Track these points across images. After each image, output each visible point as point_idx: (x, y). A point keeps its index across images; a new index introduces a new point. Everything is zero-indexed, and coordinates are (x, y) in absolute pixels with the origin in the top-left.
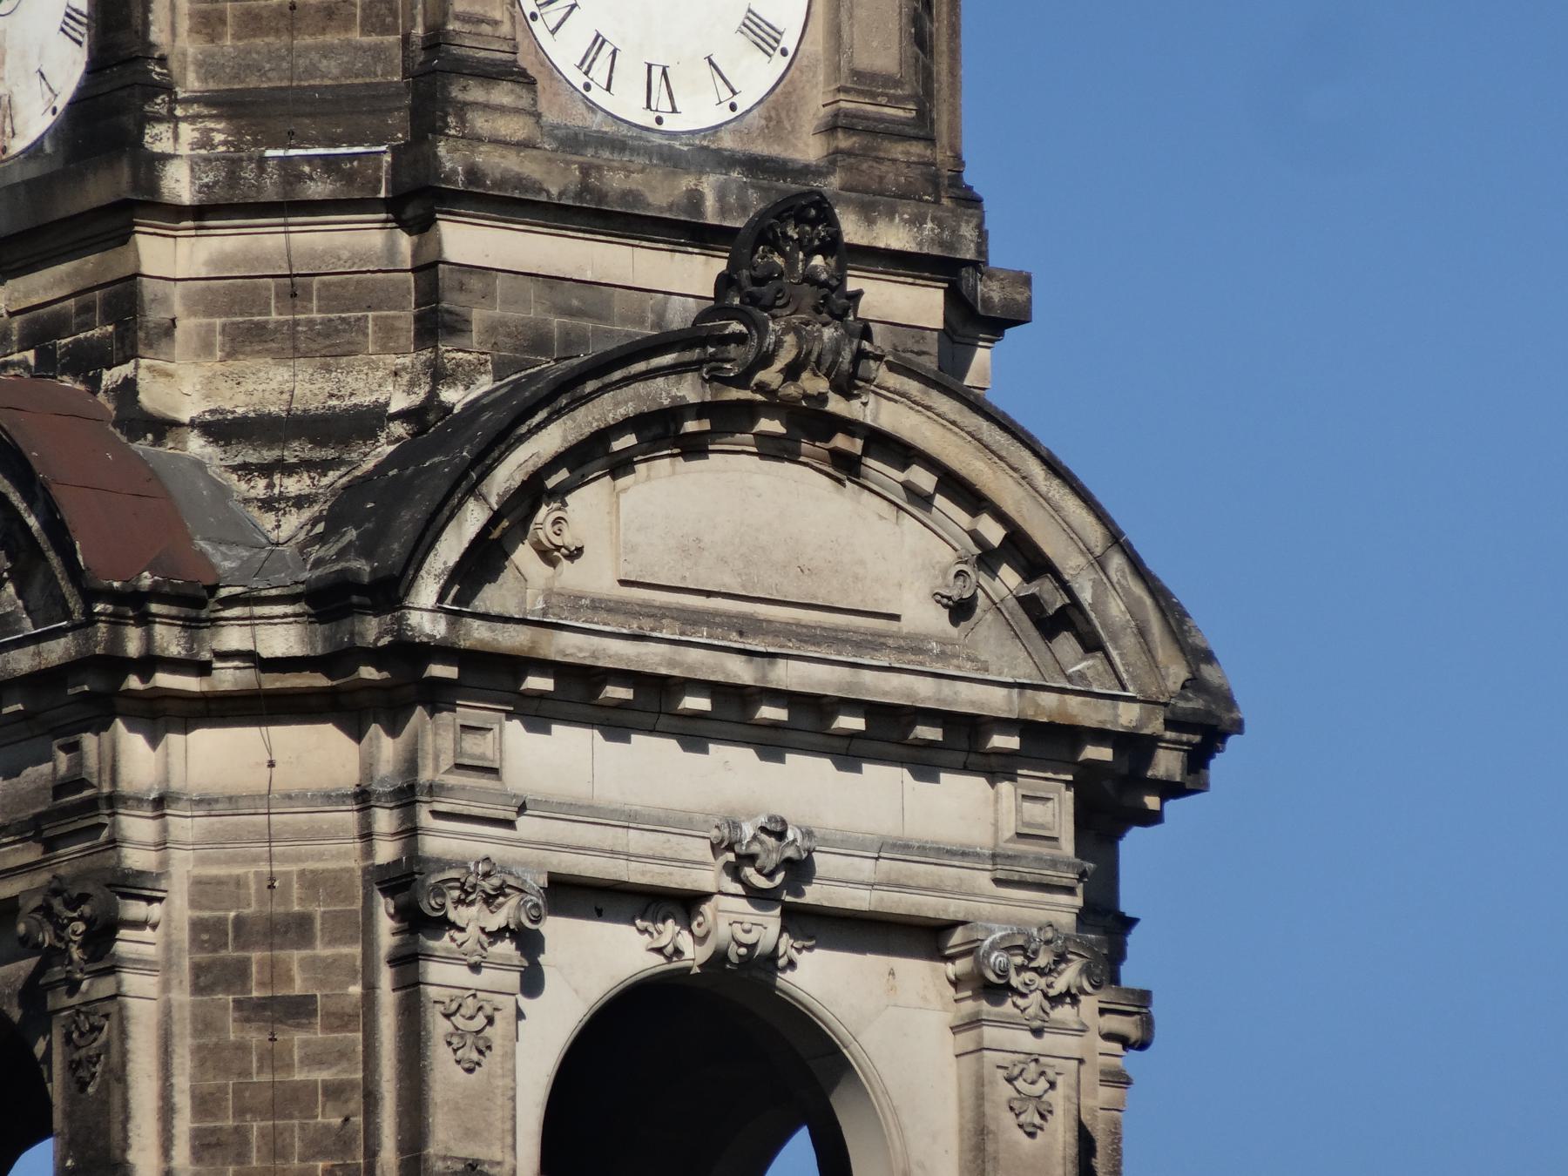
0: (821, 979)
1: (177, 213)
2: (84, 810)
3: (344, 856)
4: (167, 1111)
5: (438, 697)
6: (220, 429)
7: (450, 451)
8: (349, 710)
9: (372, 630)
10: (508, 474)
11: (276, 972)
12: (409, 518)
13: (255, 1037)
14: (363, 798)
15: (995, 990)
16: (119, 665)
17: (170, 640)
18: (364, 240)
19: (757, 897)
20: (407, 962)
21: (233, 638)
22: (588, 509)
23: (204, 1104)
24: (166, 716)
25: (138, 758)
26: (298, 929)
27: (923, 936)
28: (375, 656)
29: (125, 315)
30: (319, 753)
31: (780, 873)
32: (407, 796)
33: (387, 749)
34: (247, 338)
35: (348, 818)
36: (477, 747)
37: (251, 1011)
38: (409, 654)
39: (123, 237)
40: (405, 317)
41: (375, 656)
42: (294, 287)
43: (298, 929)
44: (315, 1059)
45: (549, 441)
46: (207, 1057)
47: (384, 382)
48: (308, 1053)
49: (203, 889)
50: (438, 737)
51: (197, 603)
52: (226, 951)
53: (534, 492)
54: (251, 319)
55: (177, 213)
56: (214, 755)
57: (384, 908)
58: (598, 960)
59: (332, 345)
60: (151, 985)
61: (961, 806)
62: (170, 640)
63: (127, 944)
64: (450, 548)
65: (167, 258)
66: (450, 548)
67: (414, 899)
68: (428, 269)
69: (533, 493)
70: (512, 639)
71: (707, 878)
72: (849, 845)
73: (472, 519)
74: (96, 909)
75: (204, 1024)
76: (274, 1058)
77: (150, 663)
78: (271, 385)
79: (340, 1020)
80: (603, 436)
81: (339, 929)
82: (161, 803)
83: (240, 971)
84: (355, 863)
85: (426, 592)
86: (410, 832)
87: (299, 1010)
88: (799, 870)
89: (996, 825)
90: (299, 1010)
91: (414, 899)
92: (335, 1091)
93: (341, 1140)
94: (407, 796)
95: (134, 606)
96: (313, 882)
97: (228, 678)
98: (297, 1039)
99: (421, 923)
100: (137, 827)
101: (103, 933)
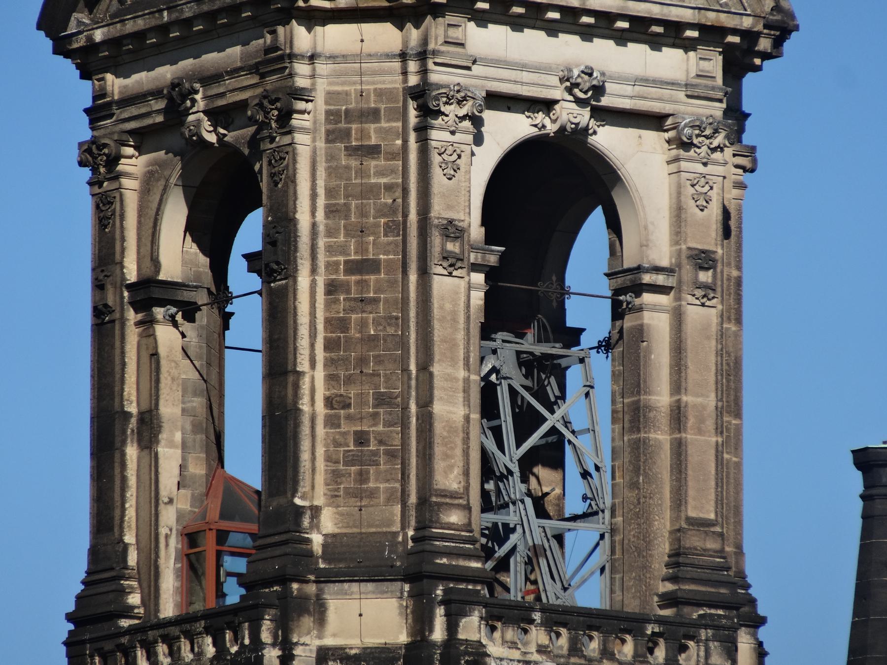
0: (608, 139)
2: (278, 60)
3: (394, 82)
4: (314, 196)
11: (363, 134)
13: (354, 163)
14: (403, 56)
15: (686, 145)
19: (579, 102)
20: (422, 130)
23: (330, 193)
25: (302, 38)
26: (374, 115)
27: (654, 121)
30: (384, 36)
31: (591, 92)
32: (423, 56)
33: (414, 35)
35: (397, 65)
36: (454, 34)
37: (353, 151)
43: (374, 115)
44: (380, 173)
46: (332, 172)
49: (331, 97)
50: (437, 29)
52: (340, 125)
56: (336, 37)
57: (412, 105)
58: (508, 130)
60: (307, 140)
61: (671, 62)
63: (297, 121)
67: (425, 101)
71: (557, 93)
72: (621, 79)
74: (283, 105)
75: (331, 157)
76: (362, 172)
79: (392, 156)
81: (392, 115)
82: (312, 58)
83: (347, 133)
84: (399, 86)
86: (424, 72)
87: (373, 151)
88: (599, 90)
89: (687, 71)
90: (373, 151)
91: (425, 101)
92: (389, 188)
94: (423, 56)
98: (372, 164)
99: (428, 113)
100: (302, 68)
101: (286, 116)
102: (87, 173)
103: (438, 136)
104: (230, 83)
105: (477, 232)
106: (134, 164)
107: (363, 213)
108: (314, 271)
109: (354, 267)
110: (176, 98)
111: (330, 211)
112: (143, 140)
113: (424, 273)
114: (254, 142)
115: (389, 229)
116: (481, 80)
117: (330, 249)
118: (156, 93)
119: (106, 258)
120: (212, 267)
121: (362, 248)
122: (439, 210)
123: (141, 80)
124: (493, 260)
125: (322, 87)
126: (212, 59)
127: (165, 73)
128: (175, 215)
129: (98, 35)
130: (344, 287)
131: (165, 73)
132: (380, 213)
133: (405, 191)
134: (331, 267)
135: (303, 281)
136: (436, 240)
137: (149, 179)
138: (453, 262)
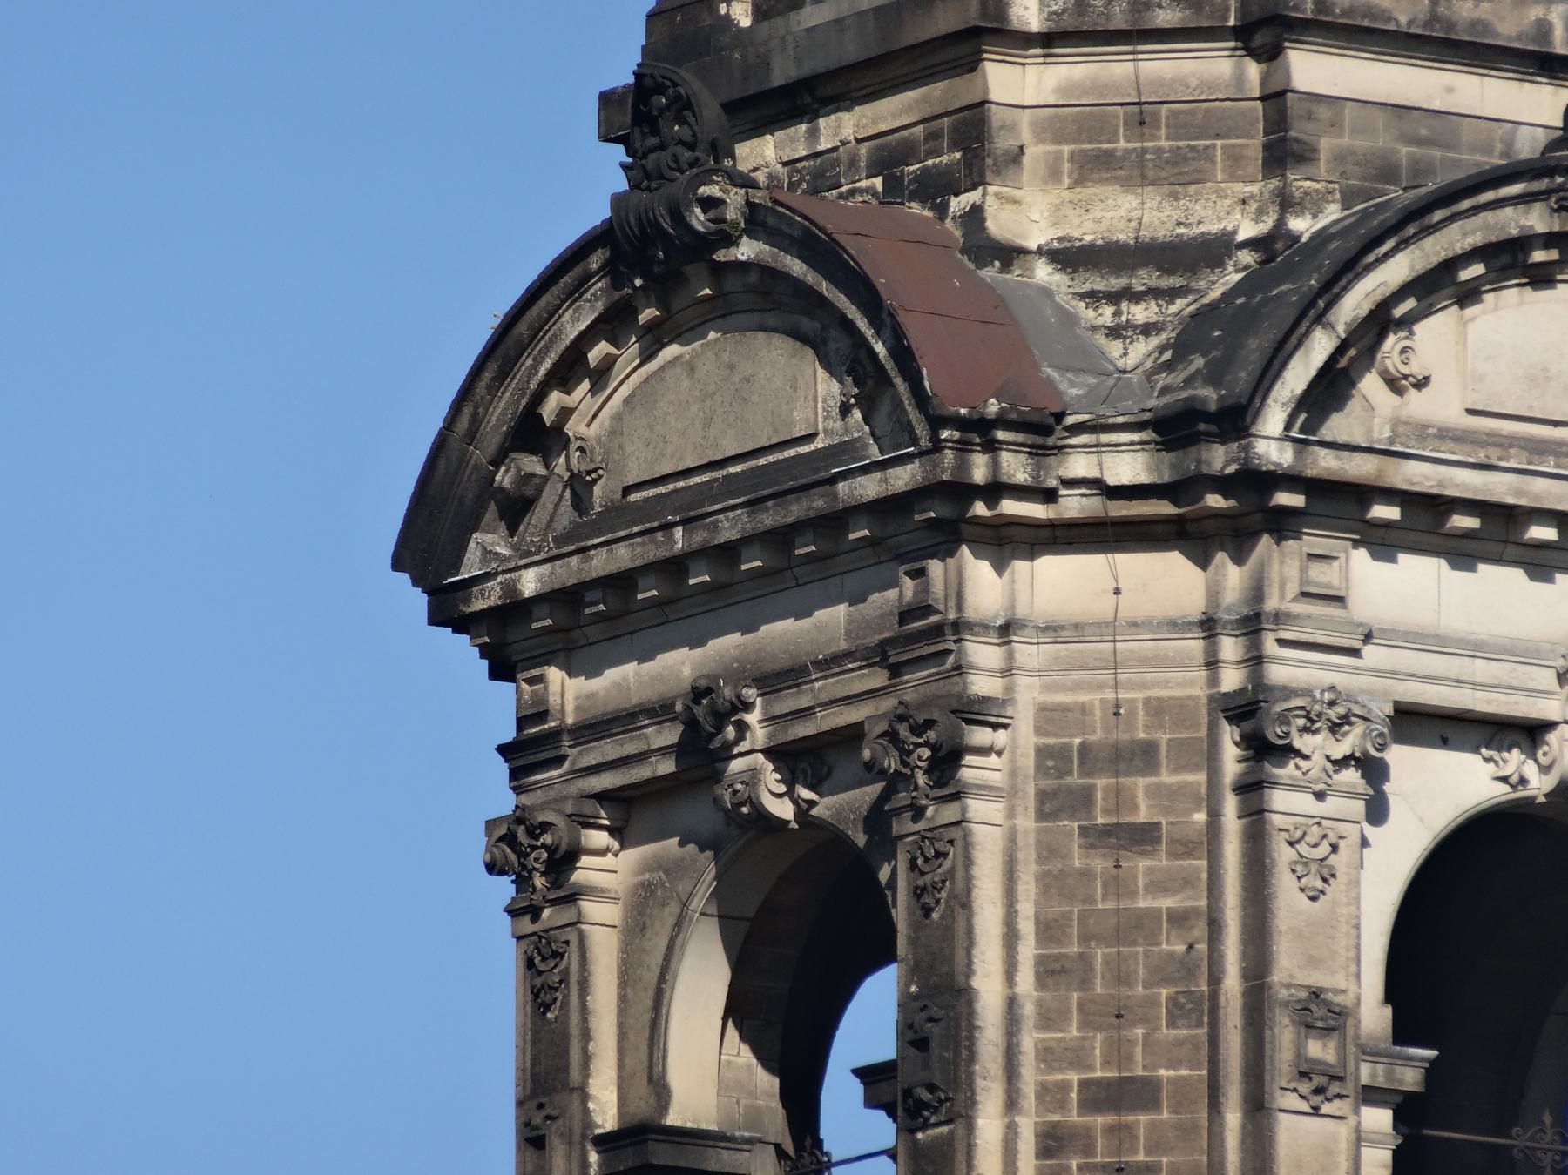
1: (1026, 40)
2: (924, 639)
3: (1189, 684)
4: (1011, 938)
5: (1283, 525)
6: (1068, 257)
7: (1296, 279)
8: (1193, 537)
9: (1219, 458)
10: (1356, 302)
11: (1121, 801)
12: (1256, 346)
13: (1100, 864)
14: (1209, 626)
16: (964, 492)
17: (1016, 468)
18: (1213, 69)
20: (1252, 789)
21: (1079, 466)
22: (1434, 339)
23: (1048, 930)
24: (1011, 542)
25: (983, 584)
26: (1143, 756)
28: (1222, 484)
29: (973, 139)
30: (1165, 580)
32: (1252, 624)
33: (1233, 577)
34: (1095, 166)
35: (1194, 645)
36: (1324, 576)
37: (1097, 838)
38: (1255, 482)
39: (972, 64)
40: (1254, 145)
41: (1222, 484)
42: (1141, 115)
43: (1143, 756)
44: (1159, 886)
45: (1396, 270)
46: (1051, 883)
47: (1231, 210)
48: (1153, 887)
49: (1048, 716)
50: (1284, 565)
51: (1043, 430)
52: (1072, 778)
53: (1380, 322)
54: (1099, 146)
55: (1026, 40)
56: (1060, 582)
57: (1229, 736)
59: (1179, 172)
62: (1016, 468)
63: (972, 770)
64: (1297, 376)
65: (1014, 85)
66: (1297, 376)
67: (1258, 726)
68: (1276, 98)
69: (1380, 322)
70: (1359, 468)
73: (1319, 348)
74: (937, 744)
75: (1048, 851)
76: (1119, 885)
77: (995, 490)
78: (1119, 213)
79: (1184, 848)
80: (1450, 265)
81: (1184, 757)
82: (1007, 630)
85: (1273, 420)
86: (1255, 660)
87: (1143, 837)
90: (1143, 837)
91: (1258, 726)
92: (1179, 919)
93: (1185, 968)
94: (1252, 624)
95: (980, 431)
96: (1157, 709)
97: (1074, 505)
98: (1142, 866)
99: (1264, 750)
100: (983, 653)
101: (947, 760)
102: (505, 888)
103: (1287, 803)
104: (825, 687)
105: (1374, 1016)
106: (609, 867)
107: (1121, 977)
108: (1012, 1104)
109: (1100, 1096)
110: (704, 722)
111: (1048, 972)
112: (630, 811)
113: (1258, 1107)
114: (877, 819)
115: (1178, 1011)
116: (1382, 679)
117: (1047, 1056)
118: (659, 711)
119: (547, 1079)
120: (786, 1096)
121: (1118, 1052)
122: (1290, 968)
123: (624, 679)
124: (1411, 1078)
125: (1028, 695)
126: (782, 634)
127: (679, 665)
128: (703, 980)
129: (530, 583)
130: (1078, 1140)
131: (679, 665)
132: (1159, 975)
133: (1215, 927)
134: (1051, 1095)
135: (988, 1126)
136: (1284, 1035)
137: (643, 903)
138: (1322, 1084)
